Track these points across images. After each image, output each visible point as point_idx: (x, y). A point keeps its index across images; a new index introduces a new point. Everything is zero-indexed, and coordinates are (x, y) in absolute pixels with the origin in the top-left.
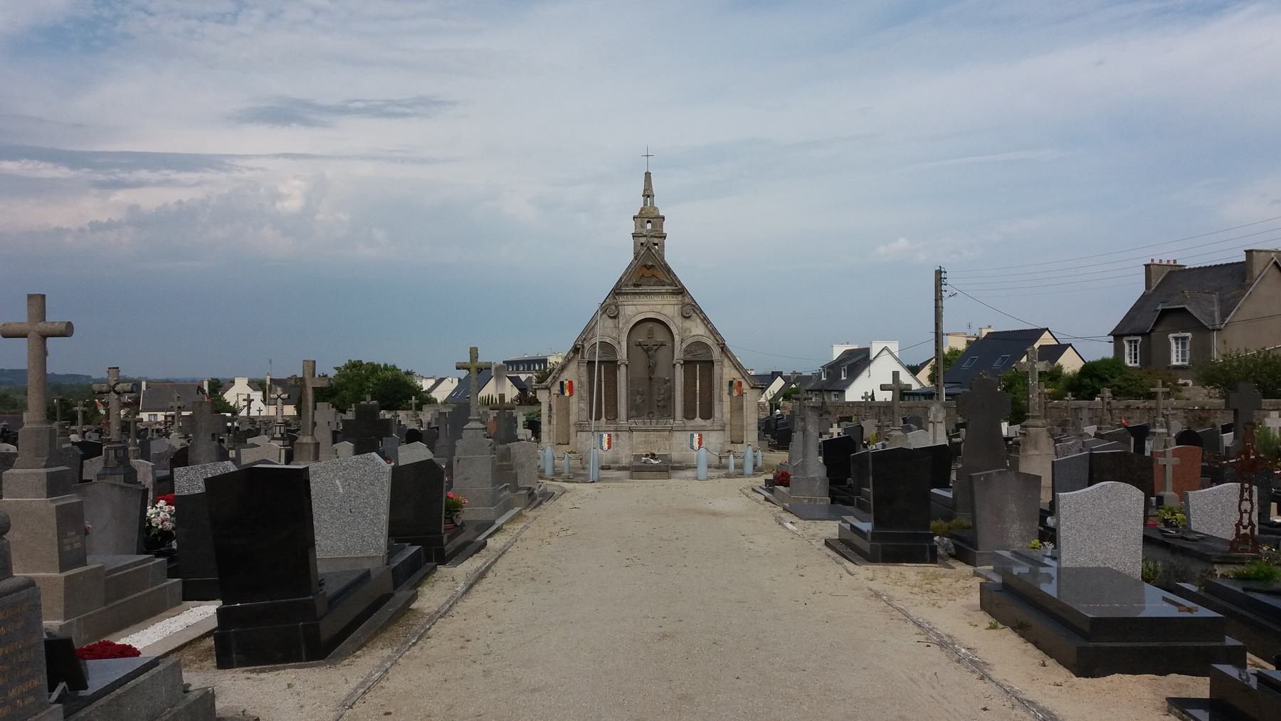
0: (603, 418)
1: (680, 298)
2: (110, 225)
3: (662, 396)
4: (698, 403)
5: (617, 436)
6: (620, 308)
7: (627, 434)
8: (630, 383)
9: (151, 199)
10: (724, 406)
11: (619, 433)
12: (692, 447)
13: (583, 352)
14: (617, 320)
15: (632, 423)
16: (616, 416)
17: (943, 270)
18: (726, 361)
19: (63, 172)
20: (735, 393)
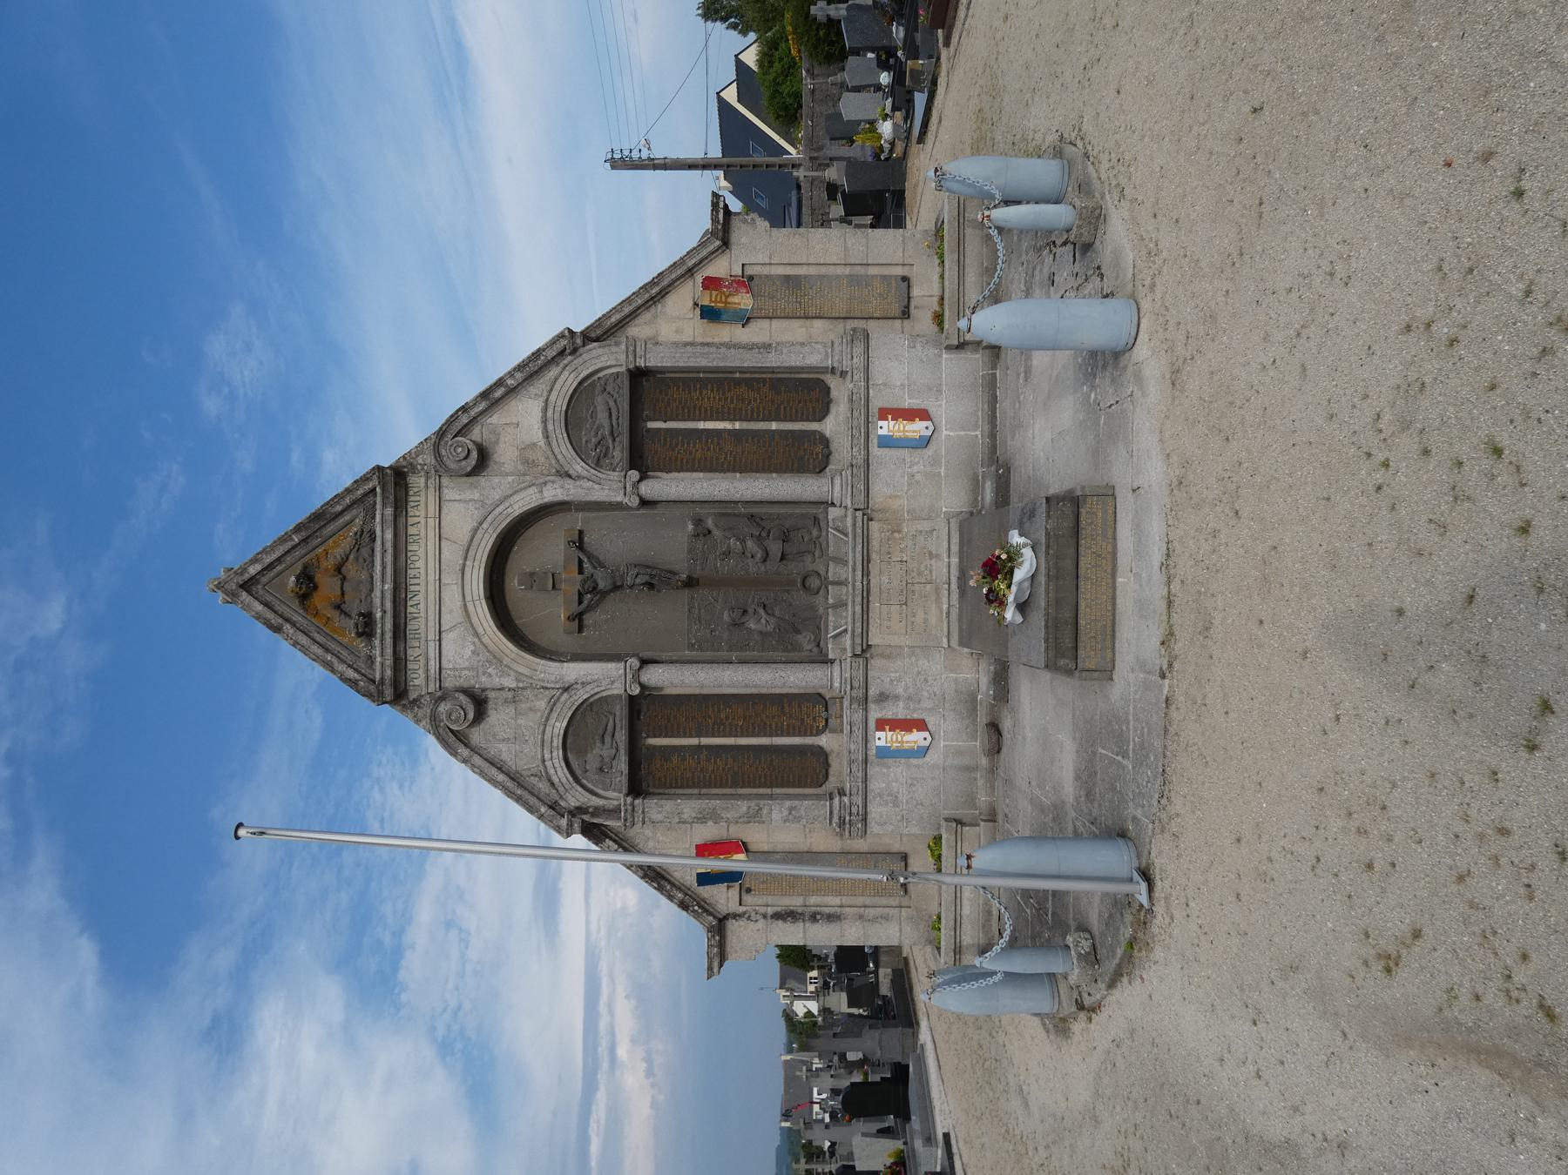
0: (824, 741)
1: (417, 482)
2: (648, 1060)
3: (750, 544)
4: (774, 426)
5: (883, 698)
6: (448, 684)
7: (876, 664)
8: (705, 652)
9: (623, 1018)
10: (787, 337)
11: (873, 692)
12: (925, 442)
13: (597, 811)
14: (491, 695)
15: (840, 646)
16: (818, 700)
17: (609, 156)
18: (638, 330)
19: (601, 1096)
20: (744, 301)
